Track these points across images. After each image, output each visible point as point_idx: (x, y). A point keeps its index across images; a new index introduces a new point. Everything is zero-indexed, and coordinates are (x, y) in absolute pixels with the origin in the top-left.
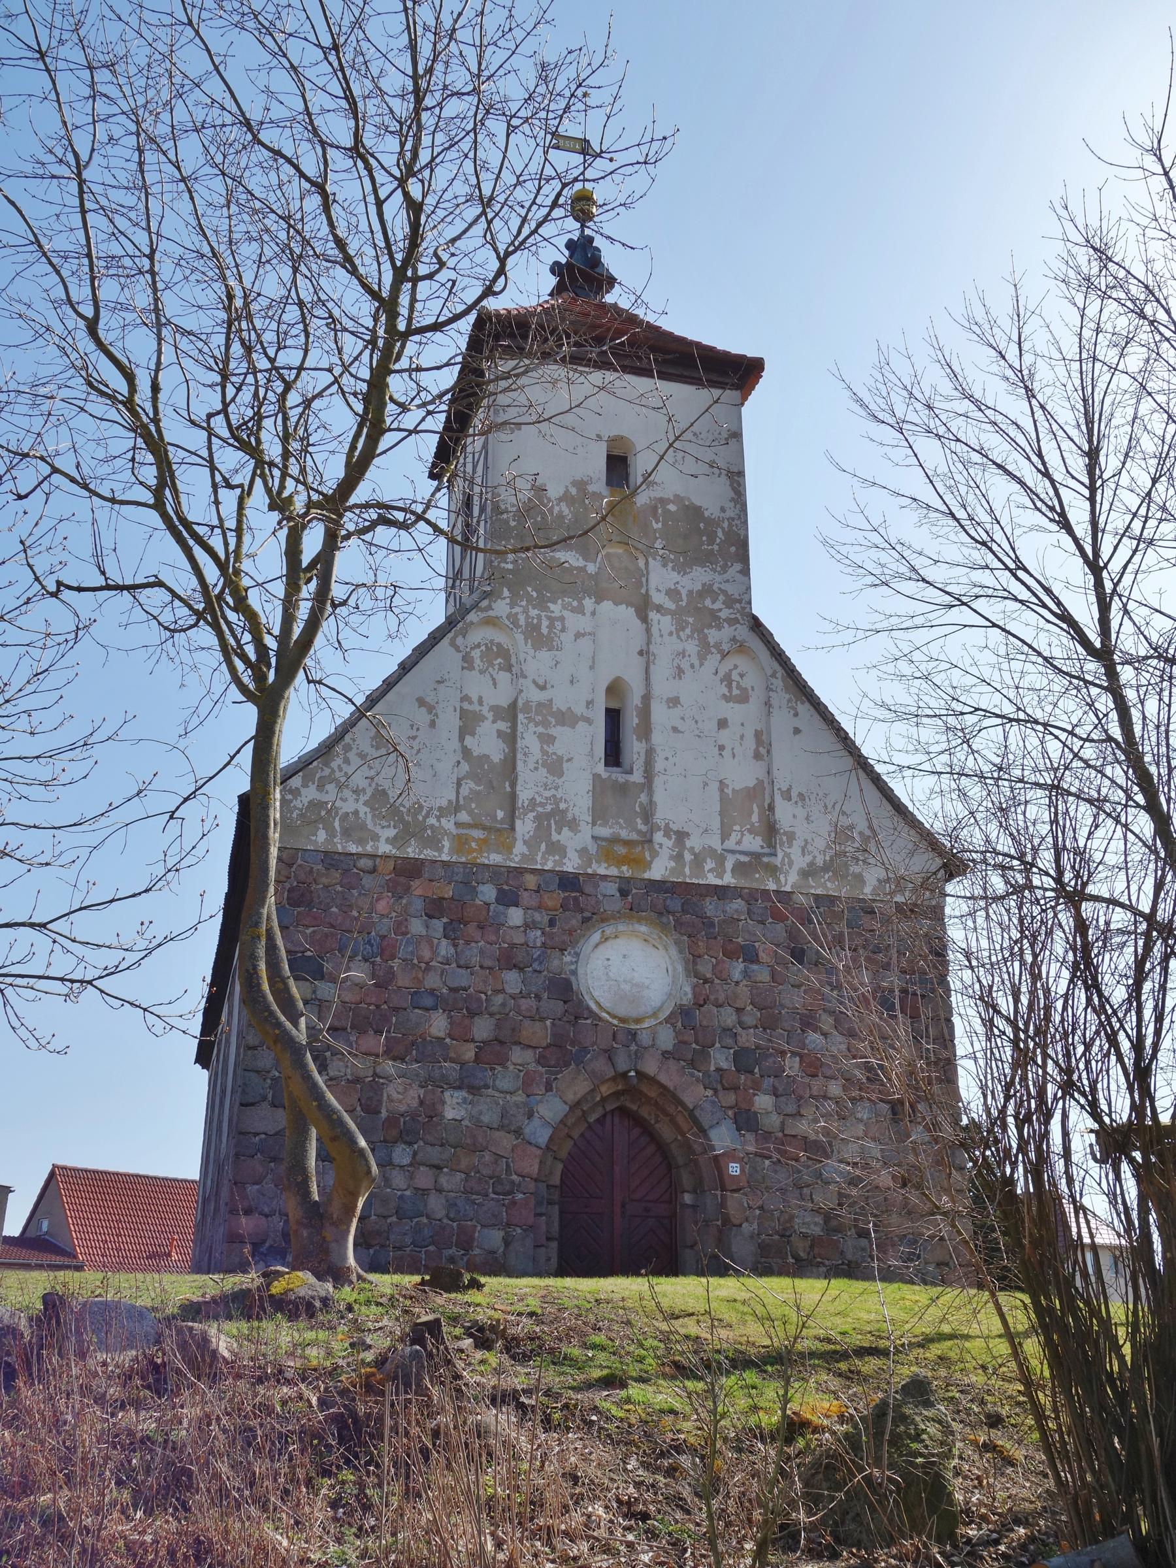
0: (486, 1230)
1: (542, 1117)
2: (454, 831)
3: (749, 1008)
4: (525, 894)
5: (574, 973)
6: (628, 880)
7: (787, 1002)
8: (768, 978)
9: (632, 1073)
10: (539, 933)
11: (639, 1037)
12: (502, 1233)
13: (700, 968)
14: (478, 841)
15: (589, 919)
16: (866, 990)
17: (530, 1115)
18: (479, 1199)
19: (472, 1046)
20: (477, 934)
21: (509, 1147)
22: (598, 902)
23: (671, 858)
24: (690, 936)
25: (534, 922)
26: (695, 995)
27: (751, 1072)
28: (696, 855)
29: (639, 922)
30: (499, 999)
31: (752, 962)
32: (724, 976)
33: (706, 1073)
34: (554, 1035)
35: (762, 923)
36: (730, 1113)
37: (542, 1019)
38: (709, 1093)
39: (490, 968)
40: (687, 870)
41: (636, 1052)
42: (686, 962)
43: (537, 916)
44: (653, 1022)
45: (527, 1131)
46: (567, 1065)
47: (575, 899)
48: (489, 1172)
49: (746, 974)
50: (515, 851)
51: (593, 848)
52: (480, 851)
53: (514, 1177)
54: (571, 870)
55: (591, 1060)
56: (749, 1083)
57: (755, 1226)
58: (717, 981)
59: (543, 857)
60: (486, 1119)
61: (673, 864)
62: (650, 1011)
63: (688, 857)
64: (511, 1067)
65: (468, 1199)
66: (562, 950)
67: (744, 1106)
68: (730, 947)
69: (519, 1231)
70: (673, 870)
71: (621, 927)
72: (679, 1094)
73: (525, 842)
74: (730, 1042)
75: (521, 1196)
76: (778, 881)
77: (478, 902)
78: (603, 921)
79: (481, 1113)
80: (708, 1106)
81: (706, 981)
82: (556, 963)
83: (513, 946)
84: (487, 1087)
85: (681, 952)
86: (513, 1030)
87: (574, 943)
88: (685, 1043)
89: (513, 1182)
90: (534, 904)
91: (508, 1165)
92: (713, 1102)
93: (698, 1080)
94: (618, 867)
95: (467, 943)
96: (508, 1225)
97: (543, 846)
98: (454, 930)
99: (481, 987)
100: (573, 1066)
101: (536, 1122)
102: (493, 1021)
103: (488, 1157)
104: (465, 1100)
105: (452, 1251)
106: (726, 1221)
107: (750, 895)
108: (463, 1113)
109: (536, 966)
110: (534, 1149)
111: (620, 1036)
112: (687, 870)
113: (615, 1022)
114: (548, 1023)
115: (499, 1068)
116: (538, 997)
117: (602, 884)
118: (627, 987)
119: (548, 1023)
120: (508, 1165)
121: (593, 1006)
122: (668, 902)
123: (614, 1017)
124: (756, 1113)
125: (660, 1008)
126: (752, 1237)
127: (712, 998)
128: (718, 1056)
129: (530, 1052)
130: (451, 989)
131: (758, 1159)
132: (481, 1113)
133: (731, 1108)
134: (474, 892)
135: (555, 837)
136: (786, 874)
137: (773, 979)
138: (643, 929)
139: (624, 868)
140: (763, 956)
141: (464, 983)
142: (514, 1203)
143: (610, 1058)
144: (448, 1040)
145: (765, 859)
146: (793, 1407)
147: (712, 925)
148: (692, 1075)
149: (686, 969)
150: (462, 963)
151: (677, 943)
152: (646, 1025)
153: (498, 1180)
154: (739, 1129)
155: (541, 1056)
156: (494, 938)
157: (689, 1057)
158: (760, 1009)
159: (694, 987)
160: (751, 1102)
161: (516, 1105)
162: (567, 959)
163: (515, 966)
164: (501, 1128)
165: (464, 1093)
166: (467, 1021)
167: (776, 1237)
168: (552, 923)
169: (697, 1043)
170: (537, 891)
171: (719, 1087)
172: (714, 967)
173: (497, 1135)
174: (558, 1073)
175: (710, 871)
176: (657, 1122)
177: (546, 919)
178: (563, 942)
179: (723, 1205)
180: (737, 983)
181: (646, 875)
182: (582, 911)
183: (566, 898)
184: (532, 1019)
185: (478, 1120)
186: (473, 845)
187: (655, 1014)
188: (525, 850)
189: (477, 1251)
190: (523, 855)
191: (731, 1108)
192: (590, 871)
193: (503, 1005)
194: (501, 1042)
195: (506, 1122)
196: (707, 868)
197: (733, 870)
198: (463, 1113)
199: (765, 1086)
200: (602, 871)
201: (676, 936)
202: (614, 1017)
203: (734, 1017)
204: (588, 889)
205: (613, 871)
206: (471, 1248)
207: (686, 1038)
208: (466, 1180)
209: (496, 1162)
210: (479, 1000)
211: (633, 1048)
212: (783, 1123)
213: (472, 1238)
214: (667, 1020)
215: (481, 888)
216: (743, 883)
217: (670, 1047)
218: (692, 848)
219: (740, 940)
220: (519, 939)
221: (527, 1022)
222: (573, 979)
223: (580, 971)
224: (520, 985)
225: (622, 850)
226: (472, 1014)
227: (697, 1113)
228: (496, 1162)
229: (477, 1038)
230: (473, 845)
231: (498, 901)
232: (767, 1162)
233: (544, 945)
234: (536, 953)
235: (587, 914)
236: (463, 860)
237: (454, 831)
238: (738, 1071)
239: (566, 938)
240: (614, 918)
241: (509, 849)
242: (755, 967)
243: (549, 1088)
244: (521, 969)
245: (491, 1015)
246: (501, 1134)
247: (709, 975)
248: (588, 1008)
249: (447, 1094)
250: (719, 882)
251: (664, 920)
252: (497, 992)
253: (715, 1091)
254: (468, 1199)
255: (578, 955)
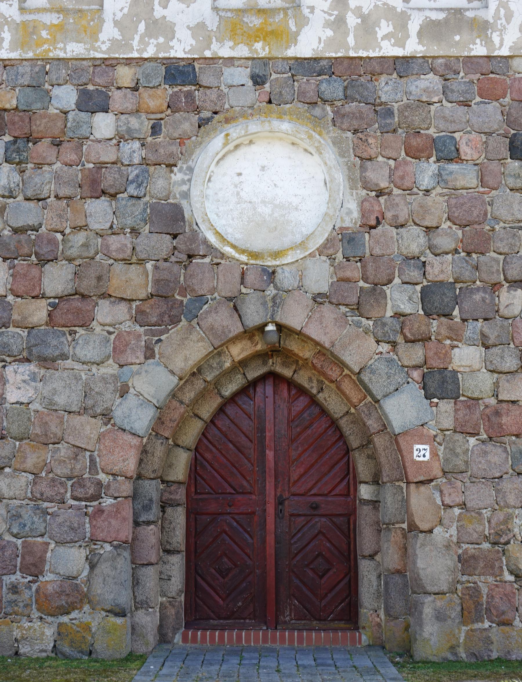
0: (61, 549)
1: (139, 394)
2: (18, 17)
3: (446, 225)
4: (116, 95)
5: (186, 195)
6: (265, 61)
7: (503, 212)
8: (474, 182)
9: (271, 327)
10: (137, 145)
11: (279, 276)
12: (83, 553)
13: (370, 175)
14: (50, 28)
15: (208, 120)
16: (87, 658)
17: (124, 391)
18: (52, 507)
19: (43, 303)
20: (51, 154)
21: (94, 436)
22: (221, 96)
23: (328, 24)
24: (355, 132)
25: (129, 130)
26: (364, 214)
27: (448, 315)
28: (365, 19)
29: (280, 117)
30: (80, 238)
31: (450, 160)
32: (407, 184)
33: (380, 322)
34: (157, 282)
35: (466, 104)
36: (416, 374)
37: (141, 262)
38: (385, 348)
39: (69, 198)
40: (351, 40)
41: (274, 298)
42: (351, 168)
43: (134, 122)
44: (299, 254)
45: (118, 414)
46: (175, 321)
47: (189, 95)
48: (66, 471)
49: (439, 176)
50: (103, 36)
51: (212, 23)
52: (54, 41)
53: (102, 477)
54: (180, 55)
55: (207, 312)
56: (444, 332)
57: (453, 531)
58: (396, 191)
59: (141, 40)
60: (61, 400)
61: (329, 33)
62: (298, 239)
63: (352, 20)
64: (98, 329)
65: (37, 508)
66: (170, 166)
67: (436, 363)
68: (415, 142)
69: (108, 547)
70: (329, 42)
71: (254, 126)
72: (337, 350)
73: (116, 23)
74: (415, 274)
75: (110, 501)
76: (488, 42)
77: (52, 111)
78: (227, 121)
79: (55, 392)
80: (382, 367)
81: (380, 193)
82: (160, 183)
83: (100, 165)
84: (64, 357)
85: (342, 154)
86: (99, 278)
87: (190, 154)
88: (347, 280)
89: (99, 484)
90: (129, 106)
91: (92, 460)
92: (390, 361)
93: (366, 332)
94: (250, 45)
95: (39, 166)
96: (93, 540)
97: (142, 27)
98: (18, 151)
99: (56, 224)
100: (184, 322)
101: (131, 400)
102: (70, 268)
103: (64, 450)
104: (33, 377)
105: (17, 577)
106: (413, 527)
107: (447, 66)
108: (31, 393)
109: (132, 190)
110: (128, 437)
111: (250, 278)
112: (351, 40)
113: (244, 258)
114: (149, 266)
115: (81, 331)
116: (135, 232)
117: (227, 71)
118: (265, 210)
119: (149, 266)
120: (92, 460)
121: (212, 239)
122: (324, 87)
123: (243, 252)
124: (455, 372)
125: (308, 237)
126: (448, 547)
127: (389, 215)
128: (396, 295)
129: (123, 307)
130: (16, 231)
131: (459, 437)
132: (55, 392)
133: (416, 367)
134: (48, 96)
135: (158, 12)
136: (502, 31)
137: (483, 182)
138: (285, 126)
139: (258, 46)
140: (466, 151)
141: (32, 221)
142: (100, 511)
143: (235, 308)
144: (10, 298)
145: (470, 14)
146: (338, 276)
147: (390, 113)
148: (358, 325)
149: (351, 179)
150: (29, 194)
151: (336, 142)
152: (289, 259)
153: (80, 482)
154: (427, 397)
155: (140, 312)
156: (74, 157)
157: (355, 300)
158: (462, 226)
159: (362, 203)
160: (447, 357)
161: (103, 379)
162: (177, 176)
163: (104, 192)
164: (84, 410)
165: (32, 367)
166: (35, 271)
167: (486, 546)
168: (155, 130)
169: (366, 281)
170: (135, 89)
171: (400, 339)
172: (392, 172)
173: (77, 420)
174: (162, 333)
175: (386, 37)
176: (321, 390)
177: (147, 125)
178: (171, 155)
179: (406, 502)
180: (427, 191)
181: (291, 53)
182: (197, 110)
183: (175, 95)
184: (127, 262)
185: (51, 403)
186: (44, 34)
187: (302, 245)
188: (116, 34)
189: (49, 577)
190: (113, 41)
191: (416, 367)
192: (208, 54)
193: (86, 245)
194: (84, 296)
195: (90, 402)
196: (380, 35)
197: (420, 34)
198: (31, 393)
199: (468, 334)
200: (225, 52)
201: (335, 132)
202: (243, 252)
203: (422, 240)
204: (205, 80)
205: (243, 51)
206: (41, 573)
207: (348, 274)
208: (35, 483)
209: (75, 457)
210: (53, 242)
211: (271, 291)
212: (496, 384)
213: (42, 560)
214: (321, 251)
215: (56, 91)
216: (435, 50)
217: (325, 288)
218: (359, 8)
219: (432, 131)
220: (109, 156)
221: (119, 267)
222: (184, 204)
223: (195, 193)
224: (110, 217)
225: (255, 21)
226: (43, 262)
227: (366, 377)
228: (75, 457)
229: (49, 292)
230: (44, 34)
231: (80, 107)
232: (472, 441)
233: (144, 162)
234: (133, 173)
235: (206, 114)
236: (30, 55)
237: (18, 17)
238: (428, 314)
239: (175, 149)
240: (243, 115)
241: (94, 35)
242: (453, 167)
243: (149, 354)
244: (113, 196)
245: (70, 260)
246: (84, 418)
247: (383, 184)
248: (205, 242)
249: (10, 369)
250: (399, 52)
251: (317, 111)
252: (78, 229)
253: (394, 344)
254: (37, 508)
255: (191, 170)
